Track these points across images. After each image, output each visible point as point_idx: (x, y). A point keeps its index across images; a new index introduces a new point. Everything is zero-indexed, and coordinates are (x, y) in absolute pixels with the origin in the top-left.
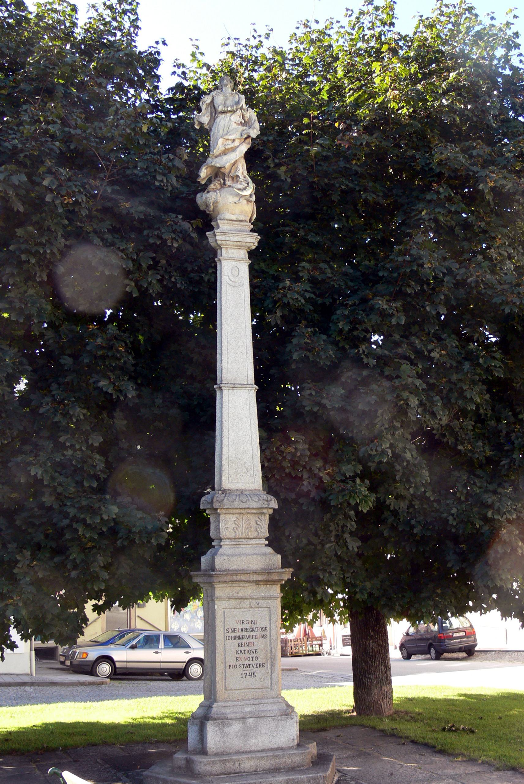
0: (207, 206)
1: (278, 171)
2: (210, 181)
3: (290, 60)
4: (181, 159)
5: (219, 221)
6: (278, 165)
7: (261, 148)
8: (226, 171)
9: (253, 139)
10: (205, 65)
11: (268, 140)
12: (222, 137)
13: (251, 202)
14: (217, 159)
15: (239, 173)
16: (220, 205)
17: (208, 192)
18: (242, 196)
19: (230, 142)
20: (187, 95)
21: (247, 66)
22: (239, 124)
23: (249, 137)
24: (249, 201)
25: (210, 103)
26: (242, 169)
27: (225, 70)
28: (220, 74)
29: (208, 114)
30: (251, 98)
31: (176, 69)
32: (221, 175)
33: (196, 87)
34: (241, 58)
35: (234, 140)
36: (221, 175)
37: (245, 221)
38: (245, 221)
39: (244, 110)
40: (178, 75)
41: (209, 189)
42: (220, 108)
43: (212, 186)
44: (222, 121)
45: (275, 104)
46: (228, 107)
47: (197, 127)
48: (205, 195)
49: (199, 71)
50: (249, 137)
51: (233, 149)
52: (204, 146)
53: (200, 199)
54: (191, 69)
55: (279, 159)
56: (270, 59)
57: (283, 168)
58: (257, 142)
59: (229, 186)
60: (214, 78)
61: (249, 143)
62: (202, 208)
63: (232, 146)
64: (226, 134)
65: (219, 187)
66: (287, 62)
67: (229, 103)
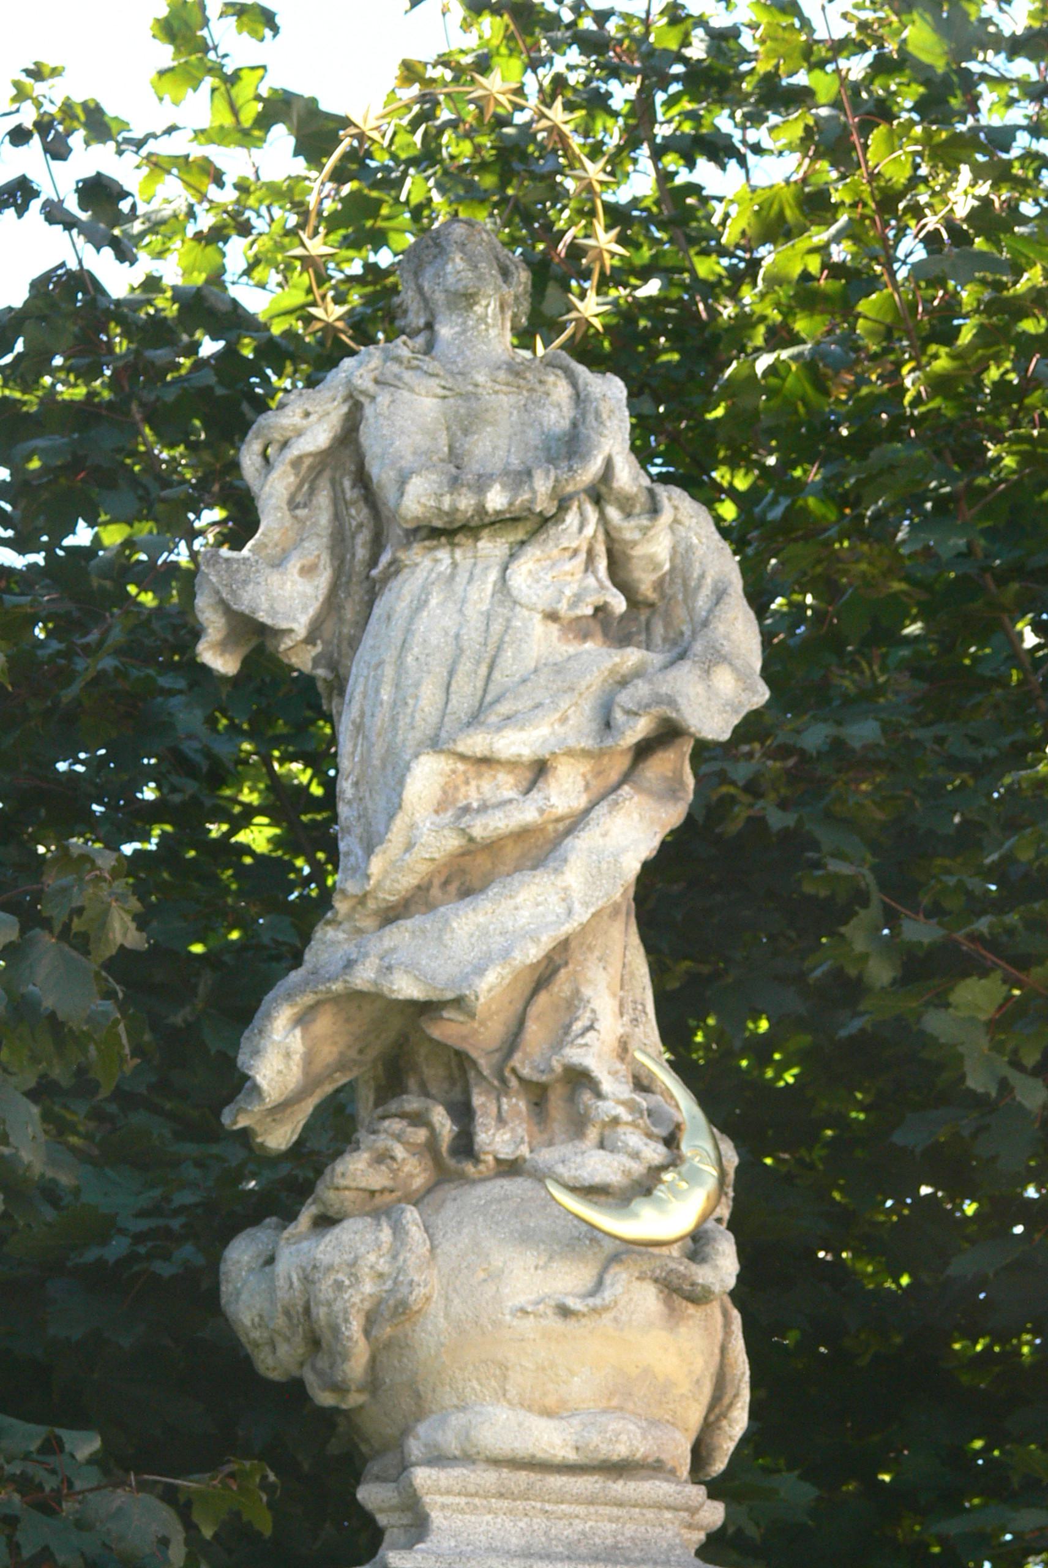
0: (315, 1343)
1: (936, 1023)
2: (335, 1125)
3: (1015, 47)
4: (83, 943)
5: (422, 1476)
6: (929, 971)
7: (778, 820)
8: (480, 1036)
9: (703, 751)
10: (280, 107)
11: (838, 745)
12: (434, 744)
13: (698, 1297)
14: (399, 935)
15: (594, 1054)
16: (433, 1331)
17: (326, 1222)
18: (628, 1250)
19: (505, 785)
20: (129, 373)
21: (642, 112)
22: (579, 629)
23: (669, 732)
24: (680, 1293)
25: (325, 460)
26: (614, 1017)
27: (456, 148)
28: (416, 186)
29: (316, 548)
30: (678, 377)
31: (30, 160)
32: (433, 1073)
33: (206, 307)
34: (592, 44)
35: (540, 770)
36: (433, 1073)
37: (655, 1468)
38: (655, 1468)
39: (626, 506)
40: (54, 214)
41: (327, 1194)
42: (418, 498)
43: (356, 1170)
44: (439, 604)
45: (895, 431)
46: (481, 485)
47: (221, 662)
48: (298, 1249)
49: (234, 162)
50: (669, 732)
51: (540, 847)
52: (284, 802)
53: (261, 1279)
54: (164, 147)
55: (936, 912)
56: (840, 47)
57: (978, 996)
58: (742, 772)
59: (511, 1168)
60: (359, 223)
61: (672, 792)
62: (276, 1361)
63: (527, 814)
64: (475, 719)
65: (415, 1172)
66: (995, 62)
67: (491, 447)
